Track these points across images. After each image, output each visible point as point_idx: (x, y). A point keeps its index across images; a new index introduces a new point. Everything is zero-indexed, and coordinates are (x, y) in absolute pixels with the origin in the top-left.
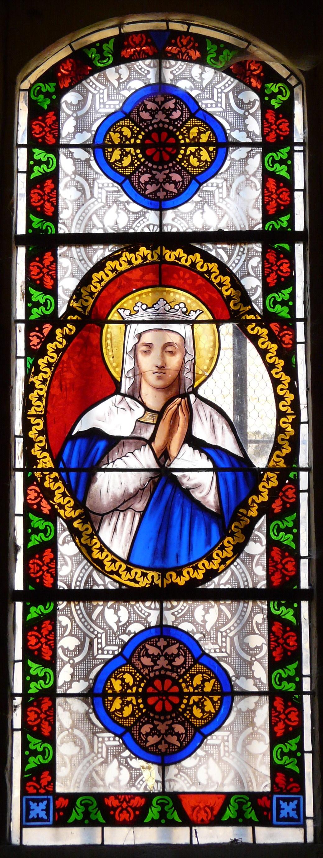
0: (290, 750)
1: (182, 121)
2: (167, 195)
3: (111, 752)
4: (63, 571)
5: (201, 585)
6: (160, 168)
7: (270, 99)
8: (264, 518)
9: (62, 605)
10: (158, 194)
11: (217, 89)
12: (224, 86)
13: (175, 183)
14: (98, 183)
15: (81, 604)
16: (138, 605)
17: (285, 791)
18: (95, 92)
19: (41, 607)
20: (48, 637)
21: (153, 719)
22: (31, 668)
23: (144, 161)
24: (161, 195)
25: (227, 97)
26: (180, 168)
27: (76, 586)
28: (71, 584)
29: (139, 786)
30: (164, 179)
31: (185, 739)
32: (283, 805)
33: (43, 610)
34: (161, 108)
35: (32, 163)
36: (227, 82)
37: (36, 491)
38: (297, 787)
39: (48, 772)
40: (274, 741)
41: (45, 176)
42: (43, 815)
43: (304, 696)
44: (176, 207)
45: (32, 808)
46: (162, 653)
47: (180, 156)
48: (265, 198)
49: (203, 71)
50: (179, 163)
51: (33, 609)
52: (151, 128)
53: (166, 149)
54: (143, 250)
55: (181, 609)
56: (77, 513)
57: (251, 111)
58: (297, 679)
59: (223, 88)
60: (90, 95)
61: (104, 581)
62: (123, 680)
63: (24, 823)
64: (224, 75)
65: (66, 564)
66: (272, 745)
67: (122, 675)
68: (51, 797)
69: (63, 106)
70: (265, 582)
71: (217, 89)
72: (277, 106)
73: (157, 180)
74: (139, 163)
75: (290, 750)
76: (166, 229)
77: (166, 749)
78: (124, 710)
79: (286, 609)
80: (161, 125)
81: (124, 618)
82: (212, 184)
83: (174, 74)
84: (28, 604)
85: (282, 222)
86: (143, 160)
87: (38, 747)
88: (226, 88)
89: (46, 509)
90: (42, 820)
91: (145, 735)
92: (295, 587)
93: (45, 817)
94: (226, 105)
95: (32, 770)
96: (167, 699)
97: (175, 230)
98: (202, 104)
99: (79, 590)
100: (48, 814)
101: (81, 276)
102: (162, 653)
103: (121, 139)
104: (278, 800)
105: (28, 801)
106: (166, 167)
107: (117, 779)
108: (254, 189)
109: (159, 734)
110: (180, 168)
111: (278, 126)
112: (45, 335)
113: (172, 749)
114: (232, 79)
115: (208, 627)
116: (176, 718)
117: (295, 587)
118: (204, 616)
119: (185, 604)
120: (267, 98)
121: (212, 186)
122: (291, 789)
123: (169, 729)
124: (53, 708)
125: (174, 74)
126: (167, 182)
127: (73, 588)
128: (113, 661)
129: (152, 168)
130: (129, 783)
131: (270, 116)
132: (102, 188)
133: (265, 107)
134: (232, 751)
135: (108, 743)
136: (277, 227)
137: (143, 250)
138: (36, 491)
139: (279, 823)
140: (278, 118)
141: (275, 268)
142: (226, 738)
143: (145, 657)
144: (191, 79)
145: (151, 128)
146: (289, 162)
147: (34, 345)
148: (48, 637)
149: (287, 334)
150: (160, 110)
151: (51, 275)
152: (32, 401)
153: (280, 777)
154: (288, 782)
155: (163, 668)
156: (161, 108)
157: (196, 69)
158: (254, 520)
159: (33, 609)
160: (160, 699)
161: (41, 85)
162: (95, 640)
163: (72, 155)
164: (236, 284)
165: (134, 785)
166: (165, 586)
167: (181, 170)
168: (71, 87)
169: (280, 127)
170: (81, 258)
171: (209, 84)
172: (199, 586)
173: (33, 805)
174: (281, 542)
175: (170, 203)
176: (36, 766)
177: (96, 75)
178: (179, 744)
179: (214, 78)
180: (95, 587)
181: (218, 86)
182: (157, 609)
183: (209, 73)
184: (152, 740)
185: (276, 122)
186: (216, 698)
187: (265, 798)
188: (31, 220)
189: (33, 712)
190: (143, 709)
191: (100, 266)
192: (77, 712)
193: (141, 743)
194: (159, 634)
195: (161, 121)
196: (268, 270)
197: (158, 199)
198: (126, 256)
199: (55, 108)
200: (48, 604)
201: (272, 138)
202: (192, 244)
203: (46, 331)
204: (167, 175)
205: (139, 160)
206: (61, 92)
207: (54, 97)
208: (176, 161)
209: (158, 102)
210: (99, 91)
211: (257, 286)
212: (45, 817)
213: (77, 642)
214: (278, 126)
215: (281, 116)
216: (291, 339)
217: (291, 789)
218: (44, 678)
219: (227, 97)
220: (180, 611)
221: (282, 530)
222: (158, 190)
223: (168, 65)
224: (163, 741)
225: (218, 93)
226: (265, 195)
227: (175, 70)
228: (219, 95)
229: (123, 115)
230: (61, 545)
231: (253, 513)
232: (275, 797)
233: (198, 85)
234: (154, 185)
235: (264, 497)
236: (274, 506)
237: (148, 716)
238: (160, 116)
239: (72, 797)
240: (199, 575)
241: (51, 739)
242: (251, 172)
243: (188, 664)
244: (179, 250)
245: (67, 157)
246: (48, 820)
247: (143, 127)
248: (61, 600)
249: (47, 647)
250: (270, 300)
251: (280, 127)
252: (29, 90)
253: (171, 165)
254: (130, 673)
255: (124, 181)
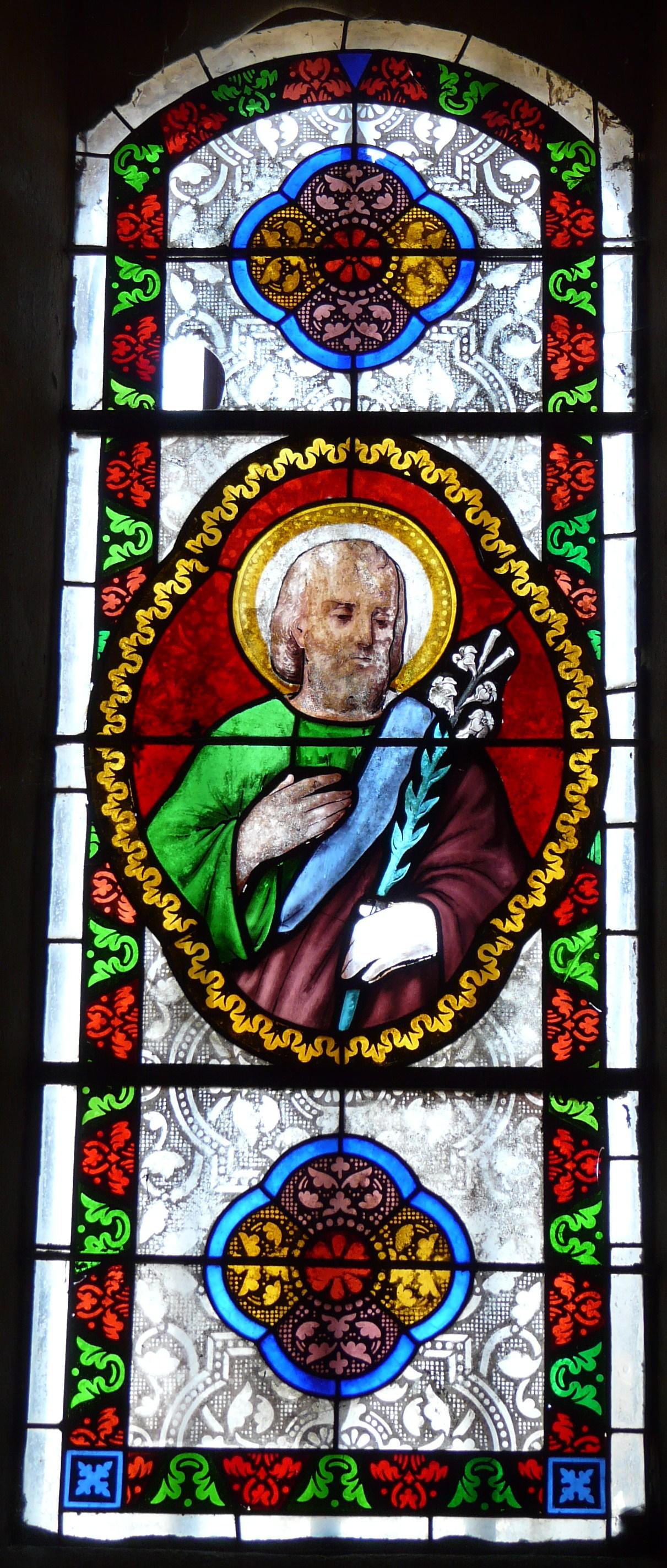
0: (583, 1370)
1: (394, 213)
2: (362, 344)
3: (238, 1369)
4: (154, 1033)
5: (418, 1060)
6: (352, 294)
7: (560, 173)
8: (538, 936)
9: (150, 1094)
10: (346, 341)
11: (462, 157)
12: (475, 151)
13: (367, 1341)
14: (215, 1341)
15: (189, 1092)
16: (298, 1096)
17: (569, 1450)
18: (234, 163)
19: (110, 1097)
20: (153, 221)
21: (320, 1310)
22: (87, 1209)
23: (324, 283)
24: (352, 342)
25: (480, 167)
26: (389, 297)
27: (177, 1058)
28: (168, 1055)
29: (292, 1434)
30: (358, 316)
31: (391, 329)
32: (568, 1476)
33: (109, 1241)
34: (343, 1186)
35: (106, 538)
36: (480, 146)
37: (109, 881)
38: (594, 1445)
39: (130, 989)
40: (552, 1352)
41: (140, 309)
42: (102, 1489)
43: (613, 1276)
44: (380, 366)
45: (81, 1474)
46: (353, 325)
47: (377, 1287)
48: (549, 350)
49: (436, 125)
50: (388, 287)
51: (94, 1102)
52: (335, 224)
53: (363, 259)
54: (319, 445)
55: (390, 119)
56: (186, 927)
57: (525, 196)
58: (592, 540)
59: (473, 155)
60: (224, 169)
61: (231, 1052)
62: (262, 1235)
63: (67, 1504)
64: (475, 132)
65: (160, 1017)
66: (549, 1359)
67: (261, 1226)
68: (120, 1455)
69: (172, 184)
70: (541, 1433)
71: (462, 157)
72: (571, 185)
73: (346, 316)
74: (313, 286)
75: (583, 1370)
76: (363, 406)
77: (358, 346)
78: (264, 1292)
79: (581, 1243)
80: (340, 1221)
81: (290, 136)
82: (444, 1343)
83: (382, 131)
84: (86, 1090)
85: (581, 271)
86: (321, 281)
87: (130, 400)
88: (478, 155)
89: (127, 914)
90: (100, 1498)
91: (304, 1341)
92: (596, 1066)
93: (107, 1494)
94: (478, 187)
95: (102, 986)
96: (359, 261)
97: (376, 408)
98: (435, 184)
99: (184, 1065)
100: (112, 1488)
101: (203, 489)
102: (353, 325)
103: (263, 1249)
104: (557, 1467)
105: (75, 1460)
106: (362, 293)
107: (250, 1422)
108: (528, 341)
109: (346, 320)
110: (389, 297)
111: (574, 345)
112: (131, 591)
113: (356, 1368)
114: (490, 140)
115: (438, 148)
116: (366, 1306)
117: (596, 1066)
118: (431, 131)
119: (398, 112)
120: (554, 170)
121: (444, 1348)
122: (583, 1445)
123: (350, 1331)
124: (129, 1284)
125: (382, 131)
126: (364, 320)
127: (172, 1061)
128: (266, 316)
129: (336, 295)
130: (272, 1428)
131: (560, 203)
132: (245, 334)
133: (550, 185)
134: (475, 353)
135: (234, 1352)
136: (571, 402)
137: (319, 445)
138: (109, 881)
139: (557, 1511)
140: (573, 207)
141: (566, 476)
142: (465, 331)
143: (307, 1192)
144: (414, 140)
145: (320, 1226)
146: (594, 285)
147: (109, 610)
148: (153, 221)
149: (586, 593)
150: (353, 321)
151: (155, 235)
152: (105, 714)
153: (563, 1423)
154: (578, 1433)
155: (353, 301)
156: (343, 1186)
157: (423, 122)
158: (519, 939)
159: (94, 1102)
160: (347, 263)
161: (134, 147)
162: (238, 170)
163: (192, 275)
164: (494, 503)
165: (282, 1433)
166: (347, 1060)
167: (391, 300)
168: (189, 150)
169: (579, 347)
170: (173, 1432)
171: (448, 146)
172: (414, 1062)
173: (85, 1469)
174: (573, 1402)
175: (369, 360)
176: (109, 976)
177: (237, 132)
178: (379, 337)
179: (455, 138)
180: (214, 1062)
181: (463, 152)
182: (335, 1105)
183: (447, 128)
184: (333, 330)
185: (570, 337)
186: (447, 260)
187: (532, 1463)
188: (91, 931)
189: (105, 881)
190: (301, 1289)
191: (236, 474)
192: (178, 1295)
193: (296, 1356)
194: (348, 157)
195: (353, 301)
196: (556, 1310)
197: (332, 1375)
198: (286, 455)
199: (158, 186)
200: (124, 1090)
201: (560, 241)
202: (409, 865)
203: (133, 585)
204: (364, 307)
205: (314, 280)
206: (170, 161)
207: (156, 170)
208: (382, 283)
209: (351, 178)
210: (240, 162)
211: (533, 176)
212: (107, 1494)
213: (178, 1161)
214: (574, 345)
215: (586, 1284)
216: (596, 1026)
217: (583, 1445)
218: (106, 1373)
219: (480, 167)
220: (388, 123)
221: (574, 1234)
222: (347, 335)
223: (371, 115)
224: (340, 1176)
225: (464, 163)
226: (548, 474)
227: (384, 123)
228: (466, 168)
229: (283, 201)
230: (172, 338)
231: (516, 925)
232: (551, 1461)
233: (416, 1390)
234: (324, 1345)
235: (539, 900)
236: (558, 914)
237: (327, 292)
238: (352, 310)
239: (160, 1458)
240: (411, 1043)
241: (123, 1346)
242: (522, 1322)
243: (390, 1206)
244: (380, 1059)
245: (183, 279)
246: (112, 1499)
247: (322, 222)
248: (149, 1085)
249: (151, 237)
250: (553, 534)
251: (579, 347)
252: (111, 157)
253: (372, 290)
254: (276, 1222)
255: (267, 1193)
